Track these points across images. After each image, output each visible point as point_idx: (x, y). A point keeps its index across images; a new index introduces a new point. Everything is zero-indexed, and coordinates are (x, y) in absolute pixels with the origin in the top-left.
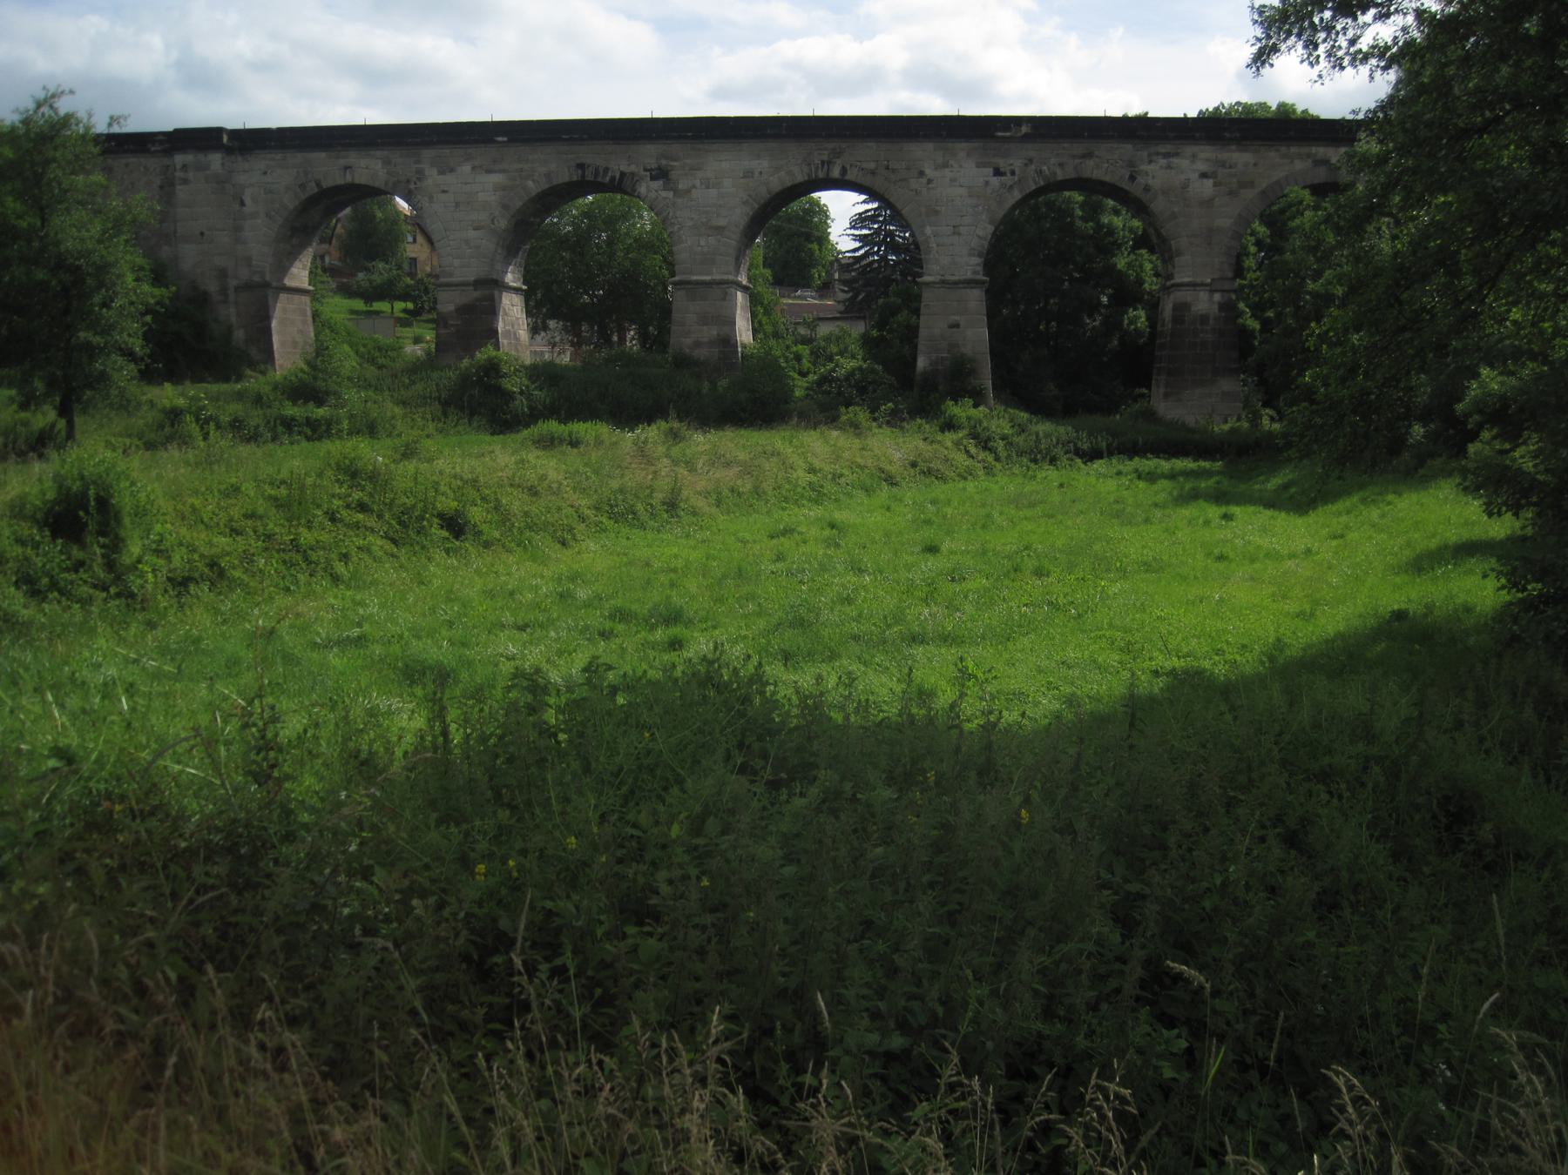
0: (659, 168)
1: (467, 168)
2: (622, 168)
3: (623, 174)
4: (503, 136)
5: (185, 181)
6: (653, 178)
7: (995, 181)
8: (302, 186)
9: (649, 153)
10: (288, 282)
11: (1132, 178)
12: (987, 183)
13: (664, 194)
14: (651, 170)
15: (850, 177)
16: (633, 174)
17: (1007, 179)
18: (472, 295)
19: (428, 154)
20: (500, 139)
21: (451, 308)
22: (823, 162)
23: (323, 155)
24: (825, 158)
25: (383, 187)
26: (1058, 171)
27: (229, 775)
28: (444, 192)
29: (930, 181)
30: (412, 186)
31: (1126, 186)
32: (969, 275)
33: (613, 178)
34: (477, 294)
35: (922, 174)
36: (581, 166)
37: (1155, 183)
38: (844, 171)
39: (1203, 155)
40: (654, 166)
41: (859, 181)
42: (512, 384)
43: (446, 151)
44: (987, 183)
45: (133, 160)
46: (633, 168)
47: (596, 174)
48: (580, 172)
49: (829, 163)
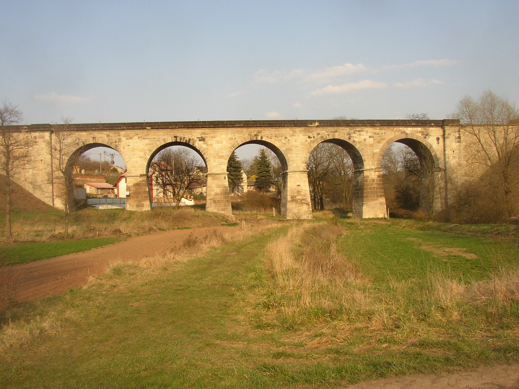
3: (190, 139)
6: (200, 141)
7: (309, 140)
11: (350, 138)
19: (122, 133)
22: (255, 135)
24: (256, 134)
26: (328, 137)
28: (128, 145)
29: (289, 140)
30: (117, 144)
33: (186, 141)
35: (286, 138)
36: (176, 137)
37: (356, 140)
38: (262, 138)
40: (200, 136)
43: (129, 132)
47: (181, 139)
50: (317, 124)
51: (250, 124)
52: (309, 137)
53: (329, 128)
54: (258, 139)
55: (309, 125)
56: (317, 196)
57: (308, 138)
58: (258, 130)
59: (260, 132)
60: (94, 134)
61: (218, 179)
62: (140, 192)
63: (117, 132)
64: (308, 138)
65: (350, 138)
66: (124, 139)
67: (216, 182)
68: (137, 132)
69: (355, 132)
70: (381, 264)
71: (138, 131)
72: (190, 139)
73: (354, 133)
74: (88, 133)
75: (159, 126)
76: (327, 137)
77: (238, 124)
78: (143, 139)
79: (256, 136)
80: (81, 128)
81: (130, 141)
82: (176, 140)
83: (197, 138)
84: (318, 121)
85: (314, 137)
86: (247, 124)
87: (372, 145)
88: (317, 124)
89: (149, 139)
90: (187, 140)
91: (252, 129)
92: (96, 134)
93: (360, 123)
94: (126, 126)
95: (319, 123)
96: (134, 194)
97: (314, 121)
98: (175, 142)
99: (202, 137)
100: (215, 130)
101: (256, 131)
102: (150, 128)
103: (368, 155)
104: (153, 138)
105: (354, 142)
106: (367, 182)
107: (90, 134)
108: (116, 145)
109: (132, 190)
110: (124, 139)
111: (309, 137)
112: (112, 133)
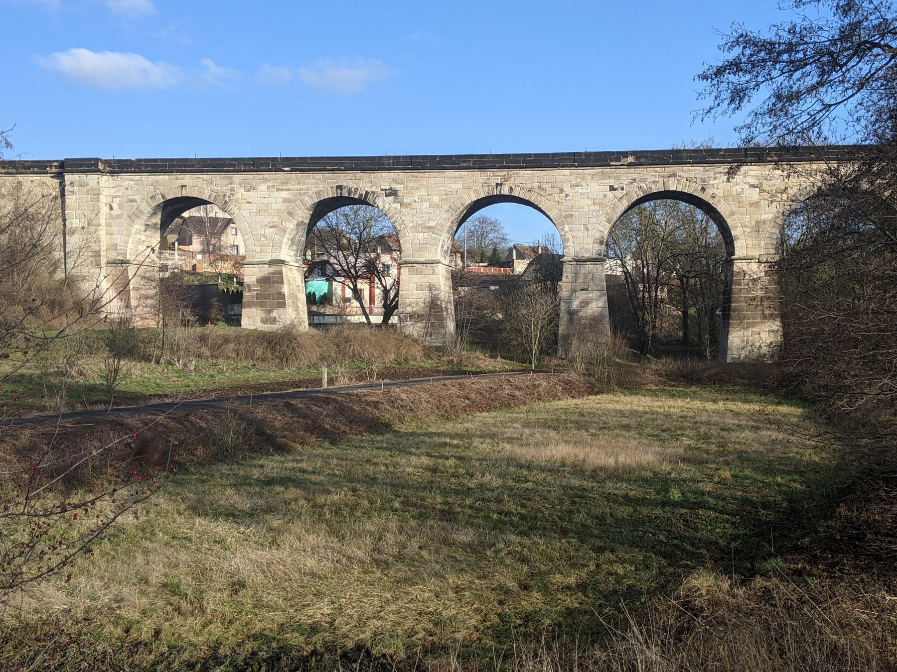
0: (391, 189)
1: (263, 187)
2: (367, 189)
3: (367, 193)
4: (288, 167)
5: (73, 192)
6: (387, 195)
7: (610, 195)
8: (152, 197)
9: (384, 179)
10: (613, 464)
11: (703, 189)
12: (605, 196)
13: (394, 205)
14: (386, 190)
15: (515, 193)
16: (374, 193)
17: (619, 194)
18: (266, 270)
19: (238, 177)
20: (286, 169)
21: (254, 279)
22: (497, 185)
23: (167, 177)
24: (499, 182)
25: (207, 199)
26: (653, 187)
27: (651, 307)
28: (248, 202)
29: (567, 196)
30: (227, 199)
31: (701, 195)
32: (594, 256)
33: (361, 195)
34: (271, 269)
35: (561, 191)
36: (340, 187)
37: (719, 193)
38: (511, 189)
39: (751, 173)
40: (388, 187)
41: (522, 196)
42: (236, 307)
43: (249, 176)
44: (605, 196)
45: (36, 178)
46: (374, 189)
47: (350, 191)
48: (339, 191)
49: (501, 184)
50: (630, 159)
51: (489, 162)
52: (612, 189)
53: (658, 169)
54: (502, 193)
55: (612, 163)
56: (628, 286)
57: (610, 190)
58: (504, 173)
59: (508, 179)
60: (183, 179)
61: (421, 273)
62: (269, 294)
63: (228, 175)
64: (610, 190)
65: (703, 189)
66: (241, 193)
67: (416, 278)
68: (265, 176)
69: (718, 175)
70: (479, 578)
71: (267, 175)
72: (367, 193)
73: (715, 178)
74: (173, 177)
75: (309, 164)
76: (651, 188)
77: (463, 162)
78: (277, 190)
79: (499, 187)
80: (159, 166)
81: (252, 193)
82: (341, 193)
83: (382, 190)
84: (633, 153)
85: (622, 189)
86: (481, 162)
87: (756, 204)
88: (630, 159)
89: (289, 190)
90: (362, 195)
91: (490, 173)
92: (188, 179)
93: (729, 156)
94: (245, 165)
95: (638, 158)
96: (257, 298)
97: (625, 154)
98: (337, 197)
99: (391, 189)
100: (416, 174)
101: (499, 176)
102: (289, 169)
103: (746, 226)
104: (297, 190)
105: (713, 197)
106: (740, 284)
107: (177, 179)
108: (226, 202)
109: (254, 290)
110: (241, 193)
111: (612, 189)
112: (216, 178)
